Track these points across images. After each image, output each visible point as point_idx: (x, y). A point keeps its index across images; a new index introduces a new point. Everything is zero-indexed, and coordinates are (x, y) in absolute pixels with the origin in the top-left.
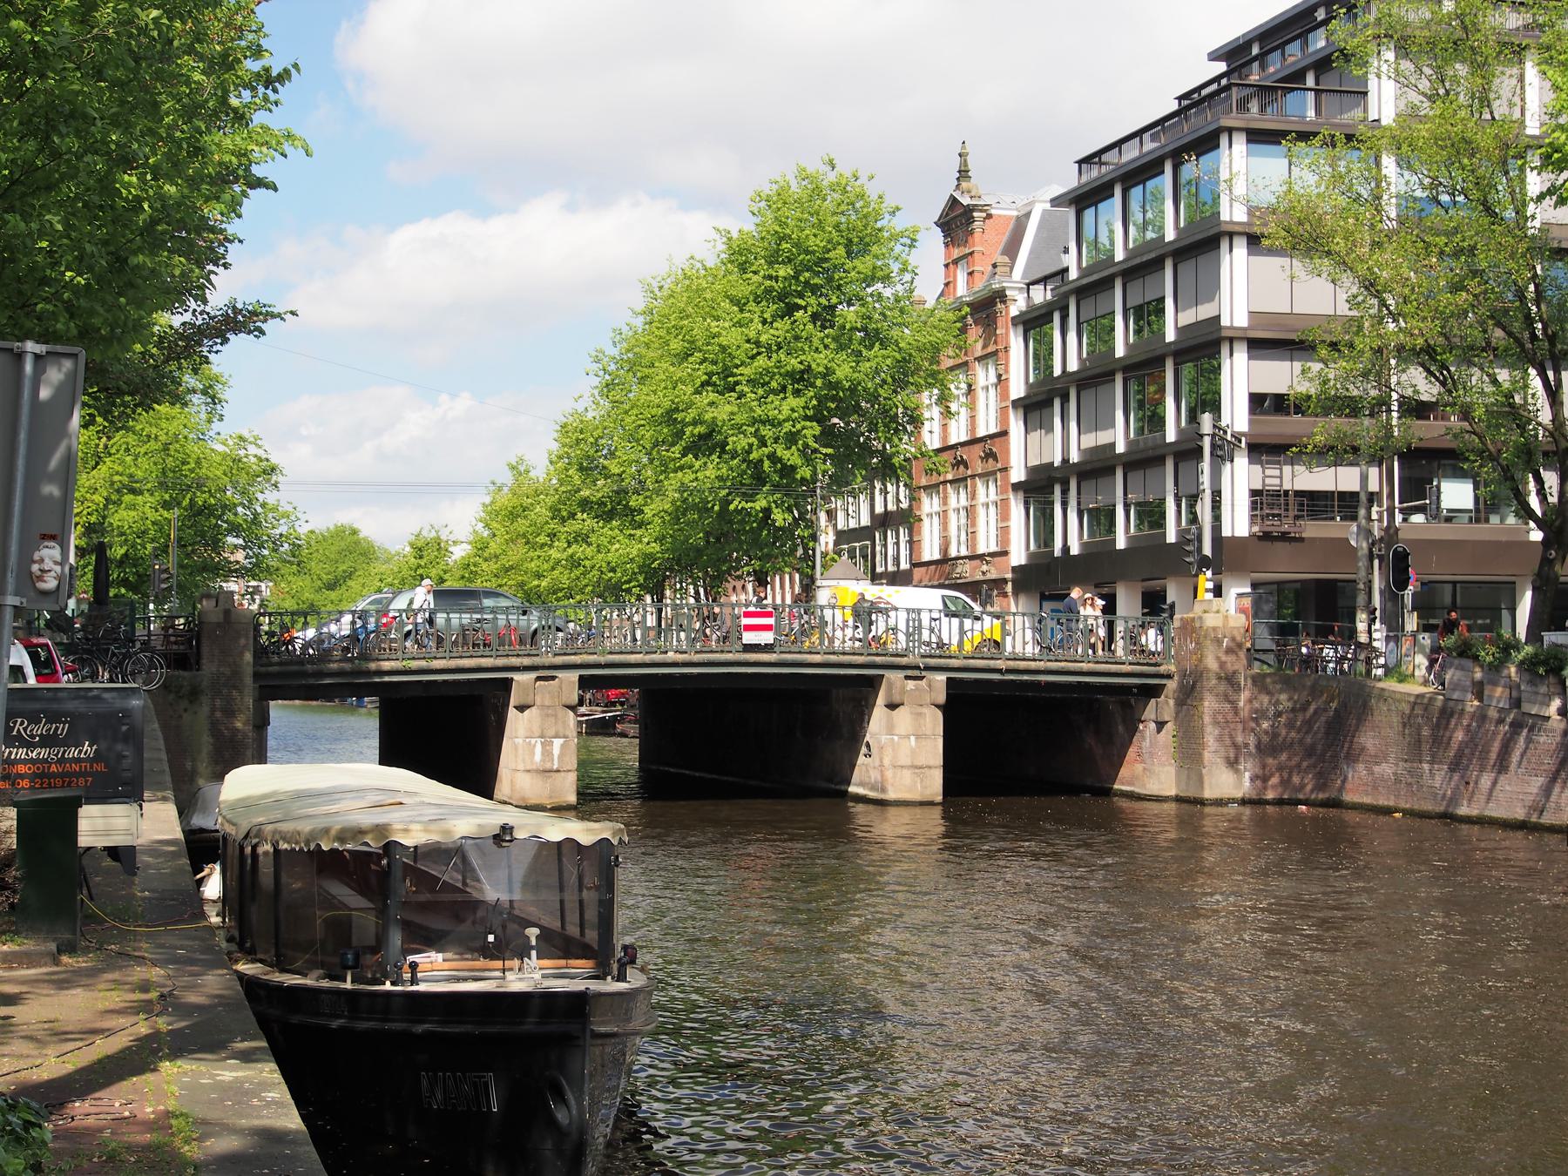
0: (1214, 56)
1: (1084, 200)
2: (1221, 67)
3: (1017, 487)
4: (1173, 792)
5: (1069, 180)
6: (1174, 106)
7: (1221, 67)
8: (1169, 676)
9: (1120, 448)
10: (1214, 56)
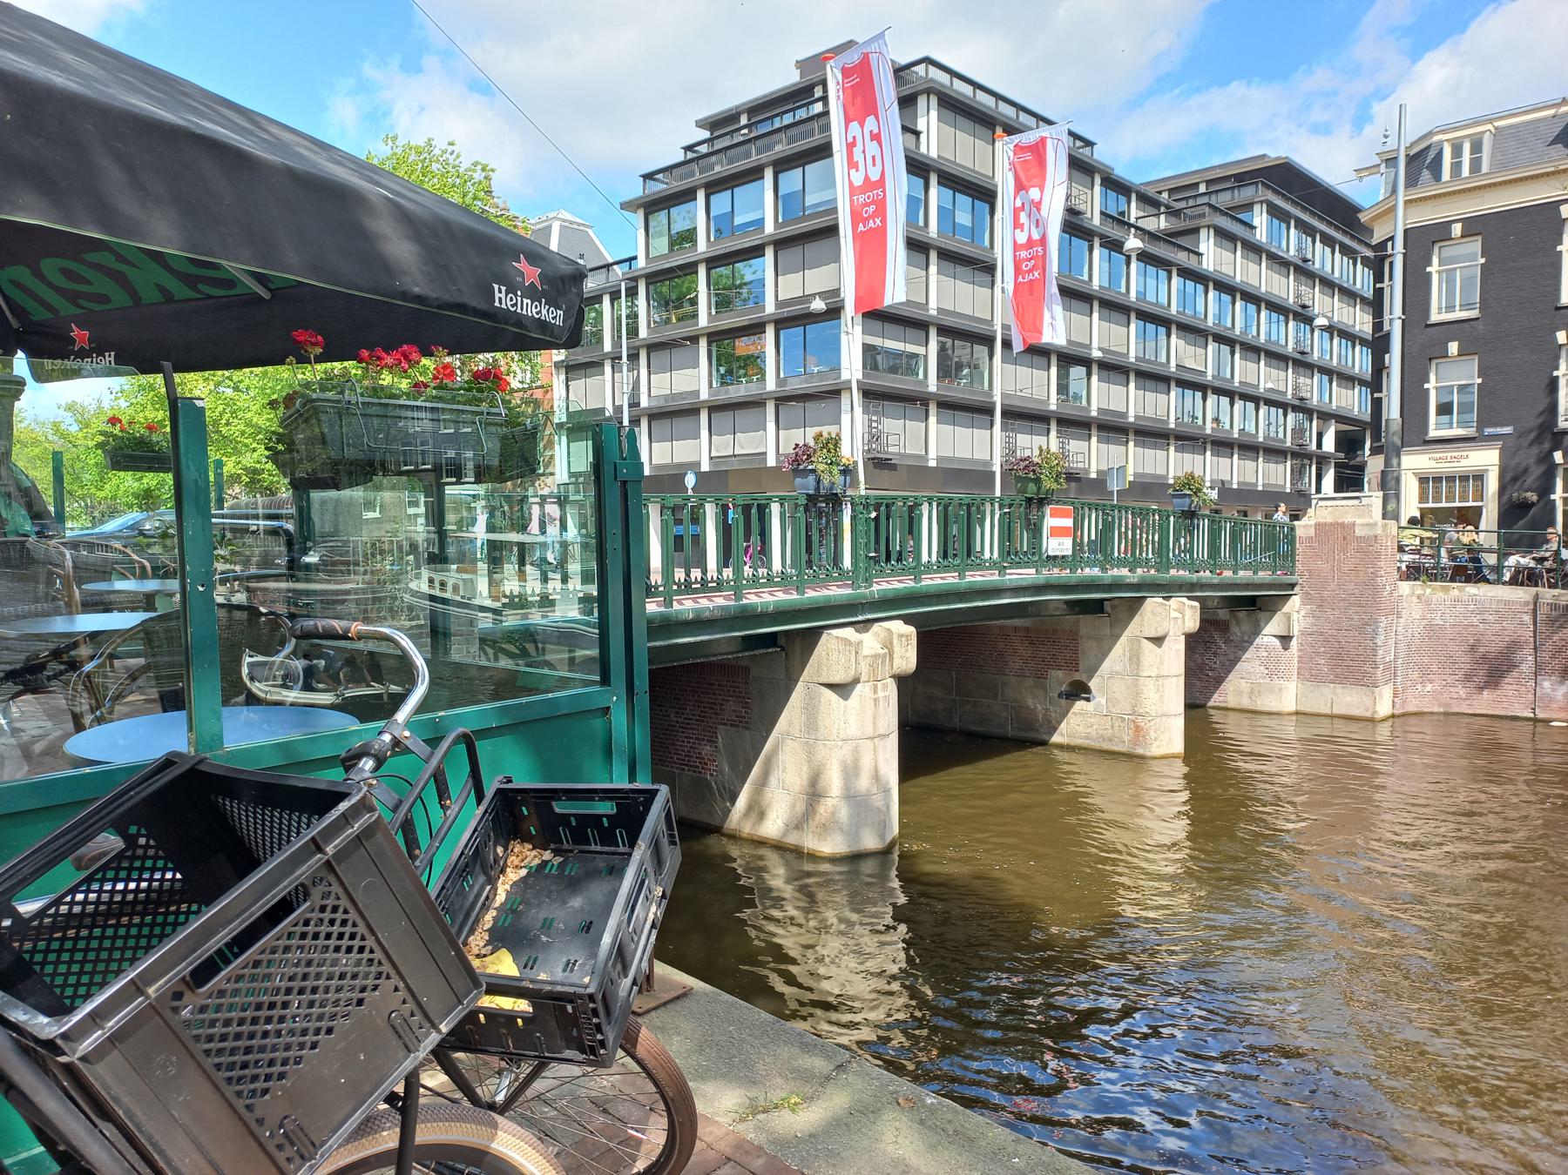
0: (701, 124)
1: (651, 206)
2: (706, 134)
3: (560, 426)
4: (1293, 708)
5: (636, 190)
6: (680, 157)
7: (706, 134)
8: (1292, 586)
9: (704, 395)
10: (701, 124)
